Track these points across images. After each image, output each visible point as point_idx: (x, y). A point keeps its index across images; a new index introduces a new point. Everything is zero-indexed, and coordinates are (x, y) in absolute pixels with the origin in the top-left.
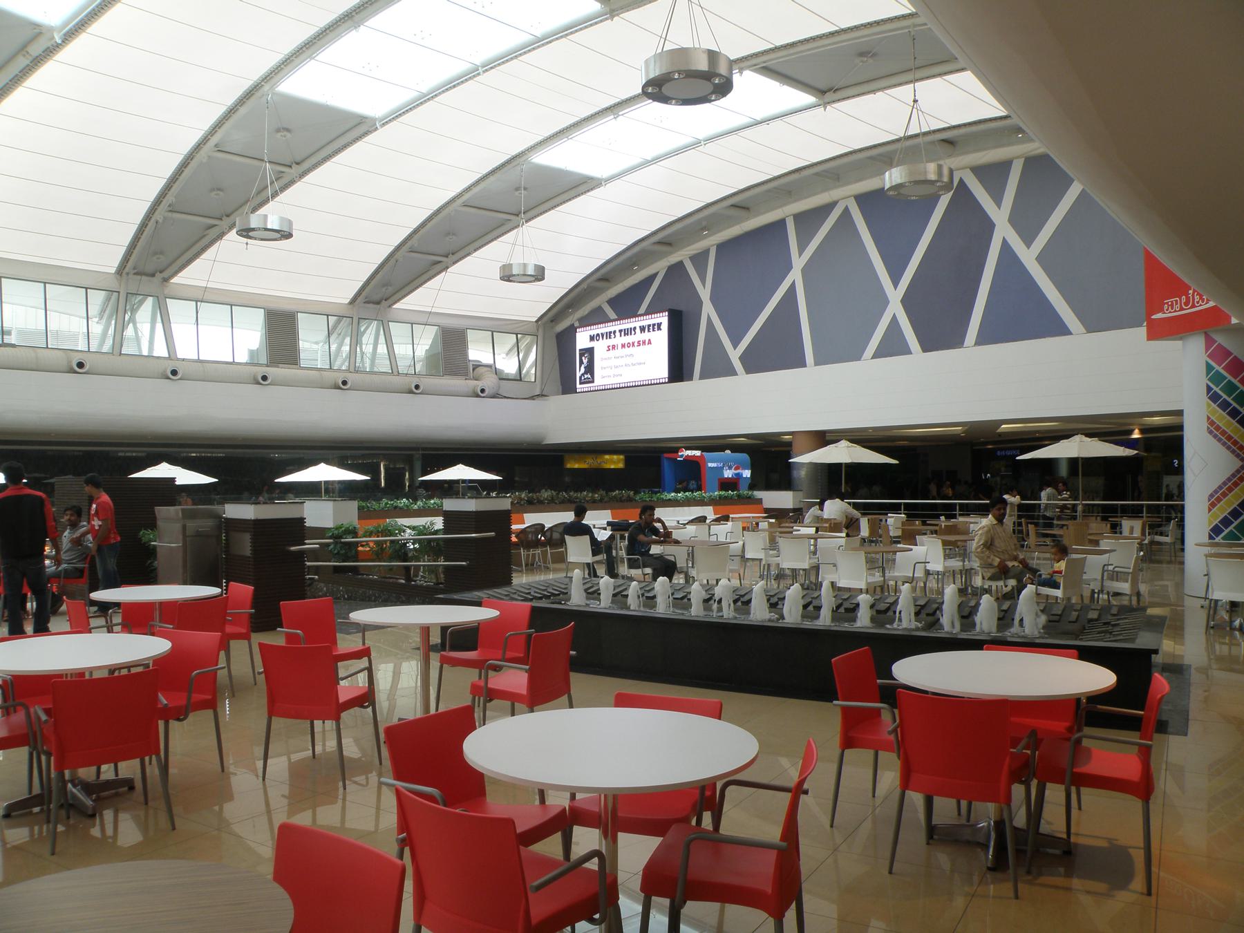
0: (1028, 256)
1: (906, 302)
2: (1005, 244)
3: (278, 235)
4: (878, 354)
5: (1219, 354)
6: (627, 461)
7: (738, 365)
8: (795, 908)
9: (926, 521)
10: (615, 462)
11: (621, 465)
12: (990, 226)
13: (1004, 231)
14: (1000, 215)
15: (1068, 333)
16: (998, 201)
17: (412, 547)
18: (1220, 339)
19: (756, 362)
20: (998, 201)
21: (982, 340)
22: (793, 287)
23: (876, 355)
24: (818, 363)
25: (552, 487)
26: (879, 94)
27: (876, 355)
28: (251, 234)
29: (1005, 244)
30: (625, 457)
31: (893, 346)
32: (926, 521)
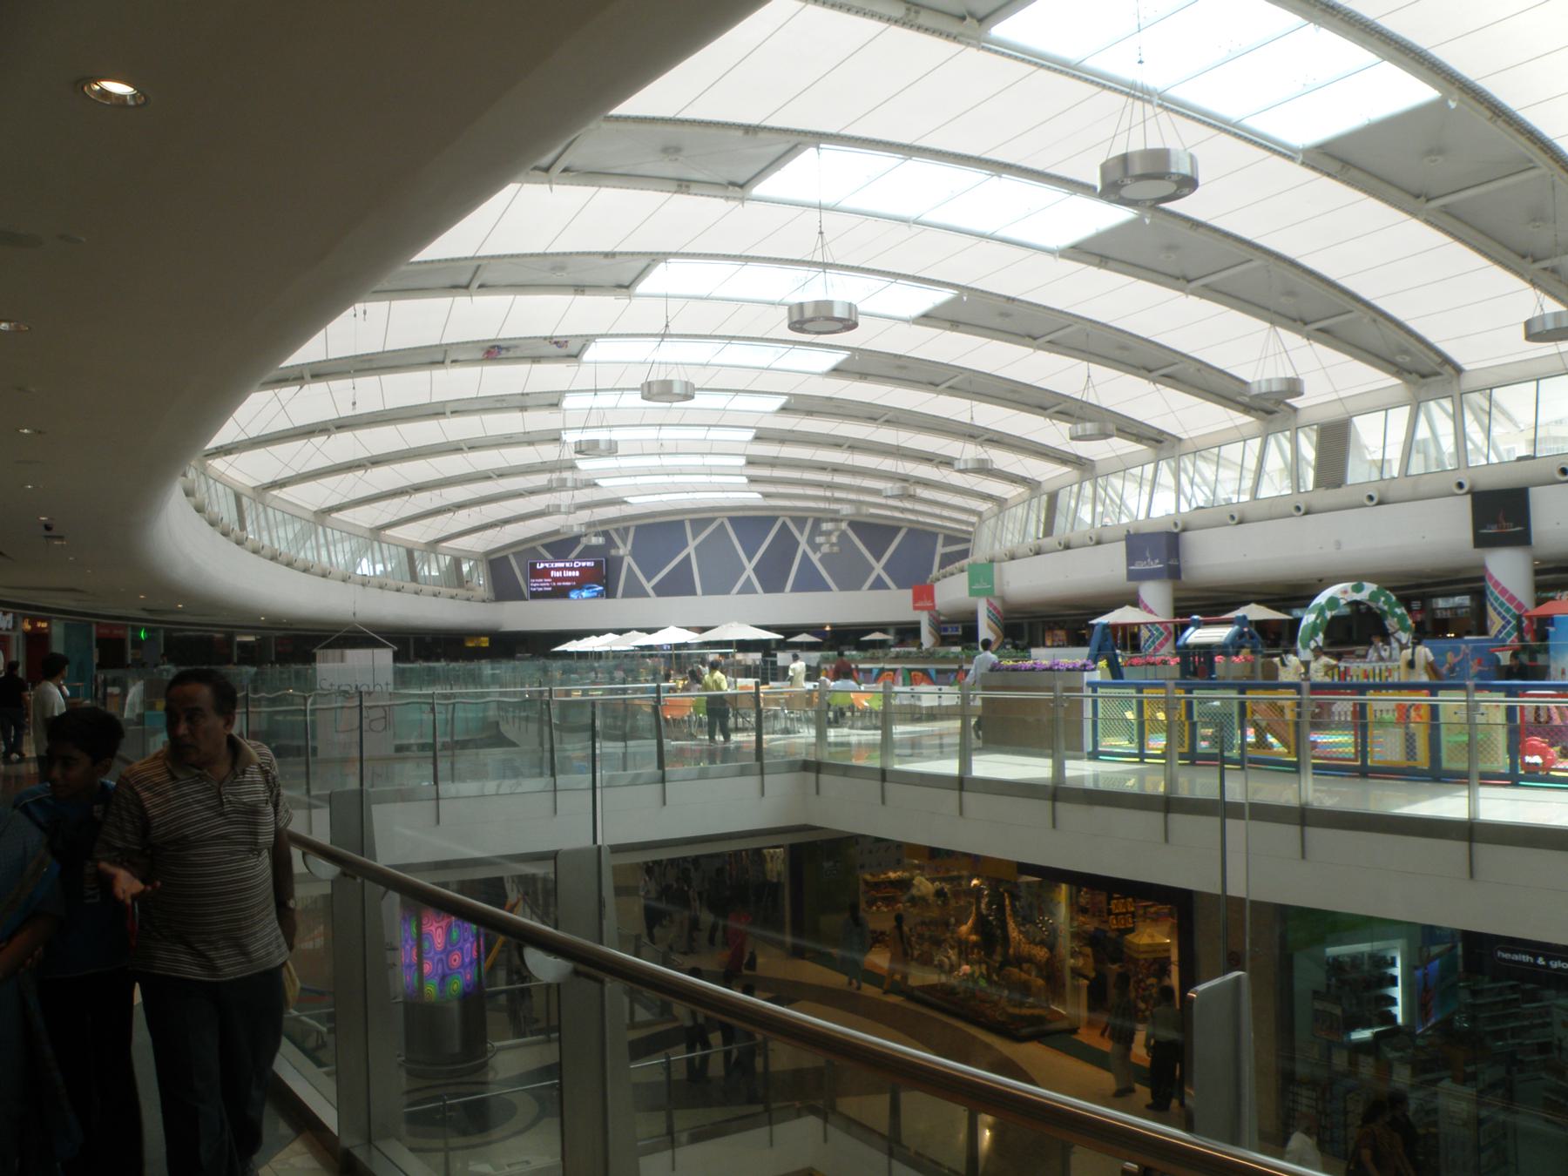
0: (815, 558)
1: (756, 570)
2: (804, 552)
3: (840, 325)
4: (739, 592)
5: (931, 615)
6: (491, 642)
7: (651, 592)
8: (230, 423)
9: (582, 695)
10: (485, 642)
11: (487, 645)
12: (797, 544)
13: (803, 546)
14: (802, 540)
15: (831, 590)
16: (802, 532)
17: (1001, 890)
18: (992, 600)
19: (663, 590)
20: (802, 532)
21: (795, 589)
22: (629, 567)
23: (739, 593)
24: (704, 593)
25: (1117, 660)
26: (1104, 406)
27: (739, 593)
28: (806, 326)
29: (804, 552)
30: (490, 639)
31: (748, 589)
32: (582, 695)
